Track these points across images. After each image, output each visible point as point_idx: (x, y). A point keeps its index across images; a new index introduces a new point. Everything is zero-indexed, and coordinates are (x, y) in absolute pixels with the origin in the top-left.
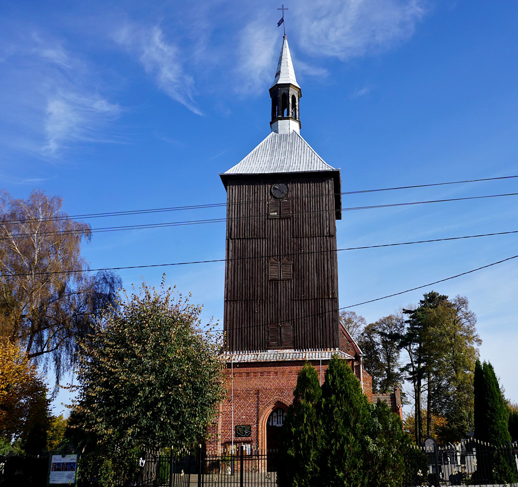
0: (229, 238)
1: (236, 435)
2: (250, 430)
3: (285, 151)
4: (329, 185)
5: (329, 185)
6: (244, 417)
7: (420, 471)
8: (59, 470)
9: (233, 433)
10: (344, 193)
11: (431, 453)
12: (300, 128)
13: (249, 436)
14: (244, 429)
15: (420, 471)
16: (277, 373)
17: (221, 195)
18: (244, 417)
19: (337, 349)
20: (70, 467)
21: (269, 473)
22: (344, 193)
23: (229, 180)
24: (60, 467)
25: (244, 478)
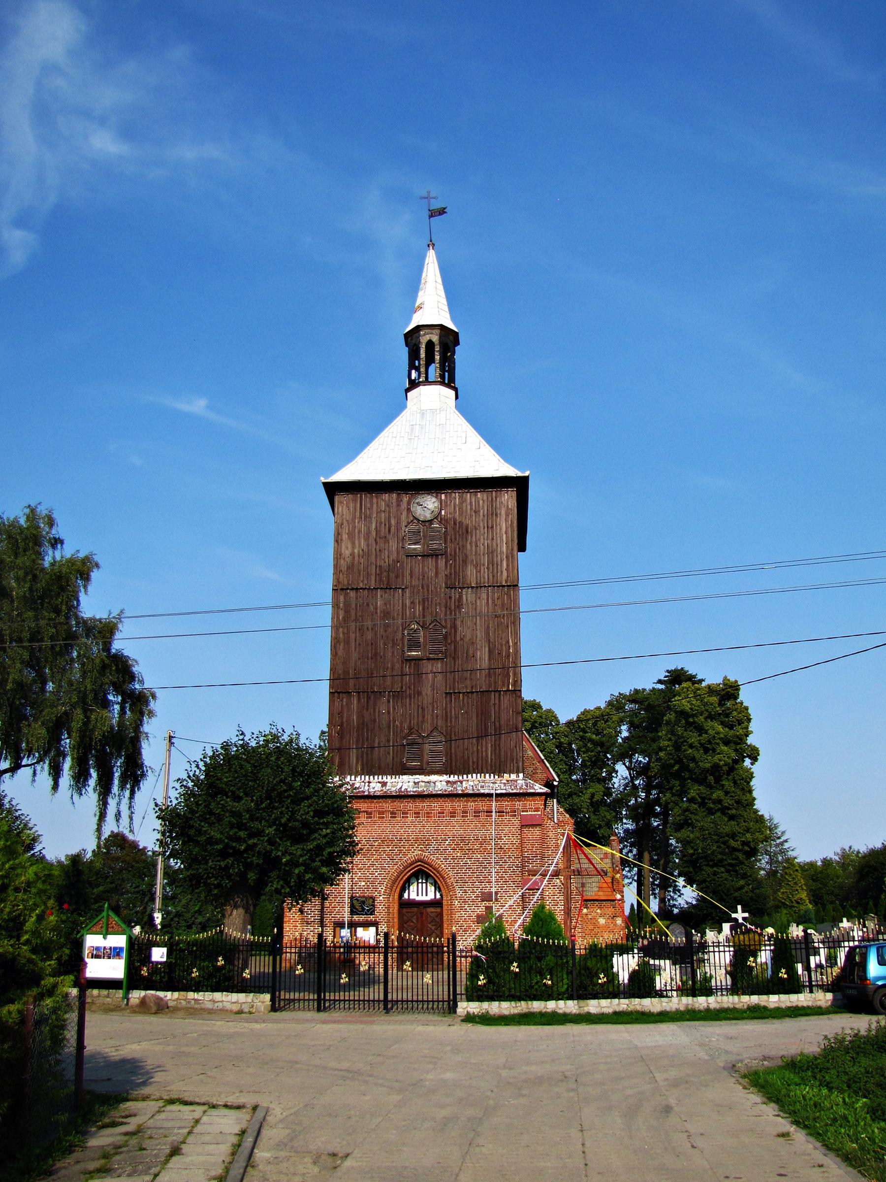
0: (339, 589)
1: (353, 912)
2: (374, 906)
3: (430, 438)
4: (508, 498)
5: (508, 498)
6: (363, 884)
7: (783, 971)
8: (97, 957)
9: (347, 909)
10: (326, 604)
11: (680, 947)
12: (457, 397)
13: (371, 914)
14: (363, 902)
15: (783, 971)
16: (419, 813)
17: (322, 517)
18: (363, 884)
19: (521, 775)
20: (115, 953)
21: (415, 973)
22: (326, 604)
23: (333, 489)
24: (98, 954)
25: (390, 977)
